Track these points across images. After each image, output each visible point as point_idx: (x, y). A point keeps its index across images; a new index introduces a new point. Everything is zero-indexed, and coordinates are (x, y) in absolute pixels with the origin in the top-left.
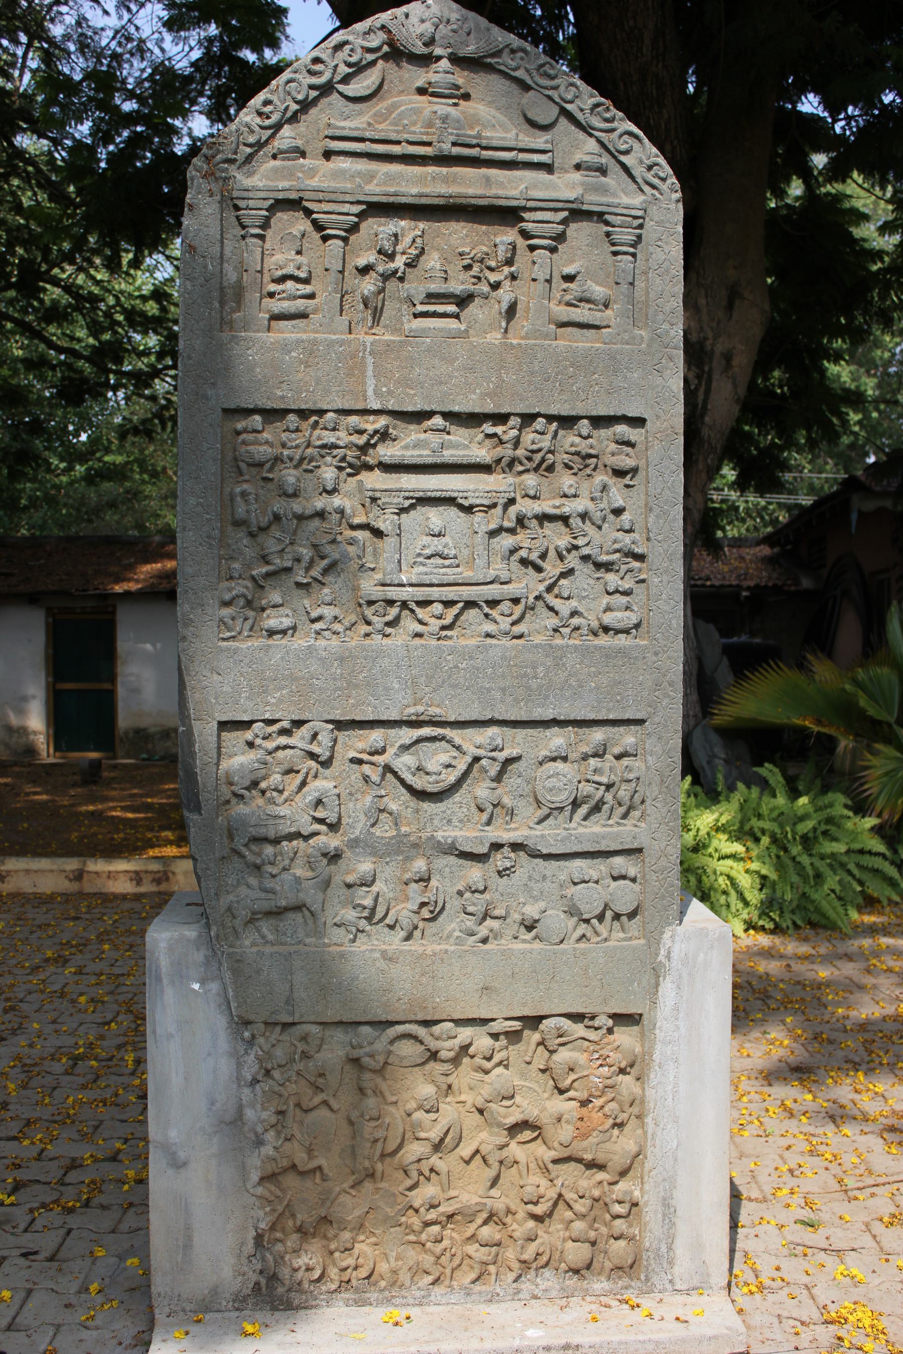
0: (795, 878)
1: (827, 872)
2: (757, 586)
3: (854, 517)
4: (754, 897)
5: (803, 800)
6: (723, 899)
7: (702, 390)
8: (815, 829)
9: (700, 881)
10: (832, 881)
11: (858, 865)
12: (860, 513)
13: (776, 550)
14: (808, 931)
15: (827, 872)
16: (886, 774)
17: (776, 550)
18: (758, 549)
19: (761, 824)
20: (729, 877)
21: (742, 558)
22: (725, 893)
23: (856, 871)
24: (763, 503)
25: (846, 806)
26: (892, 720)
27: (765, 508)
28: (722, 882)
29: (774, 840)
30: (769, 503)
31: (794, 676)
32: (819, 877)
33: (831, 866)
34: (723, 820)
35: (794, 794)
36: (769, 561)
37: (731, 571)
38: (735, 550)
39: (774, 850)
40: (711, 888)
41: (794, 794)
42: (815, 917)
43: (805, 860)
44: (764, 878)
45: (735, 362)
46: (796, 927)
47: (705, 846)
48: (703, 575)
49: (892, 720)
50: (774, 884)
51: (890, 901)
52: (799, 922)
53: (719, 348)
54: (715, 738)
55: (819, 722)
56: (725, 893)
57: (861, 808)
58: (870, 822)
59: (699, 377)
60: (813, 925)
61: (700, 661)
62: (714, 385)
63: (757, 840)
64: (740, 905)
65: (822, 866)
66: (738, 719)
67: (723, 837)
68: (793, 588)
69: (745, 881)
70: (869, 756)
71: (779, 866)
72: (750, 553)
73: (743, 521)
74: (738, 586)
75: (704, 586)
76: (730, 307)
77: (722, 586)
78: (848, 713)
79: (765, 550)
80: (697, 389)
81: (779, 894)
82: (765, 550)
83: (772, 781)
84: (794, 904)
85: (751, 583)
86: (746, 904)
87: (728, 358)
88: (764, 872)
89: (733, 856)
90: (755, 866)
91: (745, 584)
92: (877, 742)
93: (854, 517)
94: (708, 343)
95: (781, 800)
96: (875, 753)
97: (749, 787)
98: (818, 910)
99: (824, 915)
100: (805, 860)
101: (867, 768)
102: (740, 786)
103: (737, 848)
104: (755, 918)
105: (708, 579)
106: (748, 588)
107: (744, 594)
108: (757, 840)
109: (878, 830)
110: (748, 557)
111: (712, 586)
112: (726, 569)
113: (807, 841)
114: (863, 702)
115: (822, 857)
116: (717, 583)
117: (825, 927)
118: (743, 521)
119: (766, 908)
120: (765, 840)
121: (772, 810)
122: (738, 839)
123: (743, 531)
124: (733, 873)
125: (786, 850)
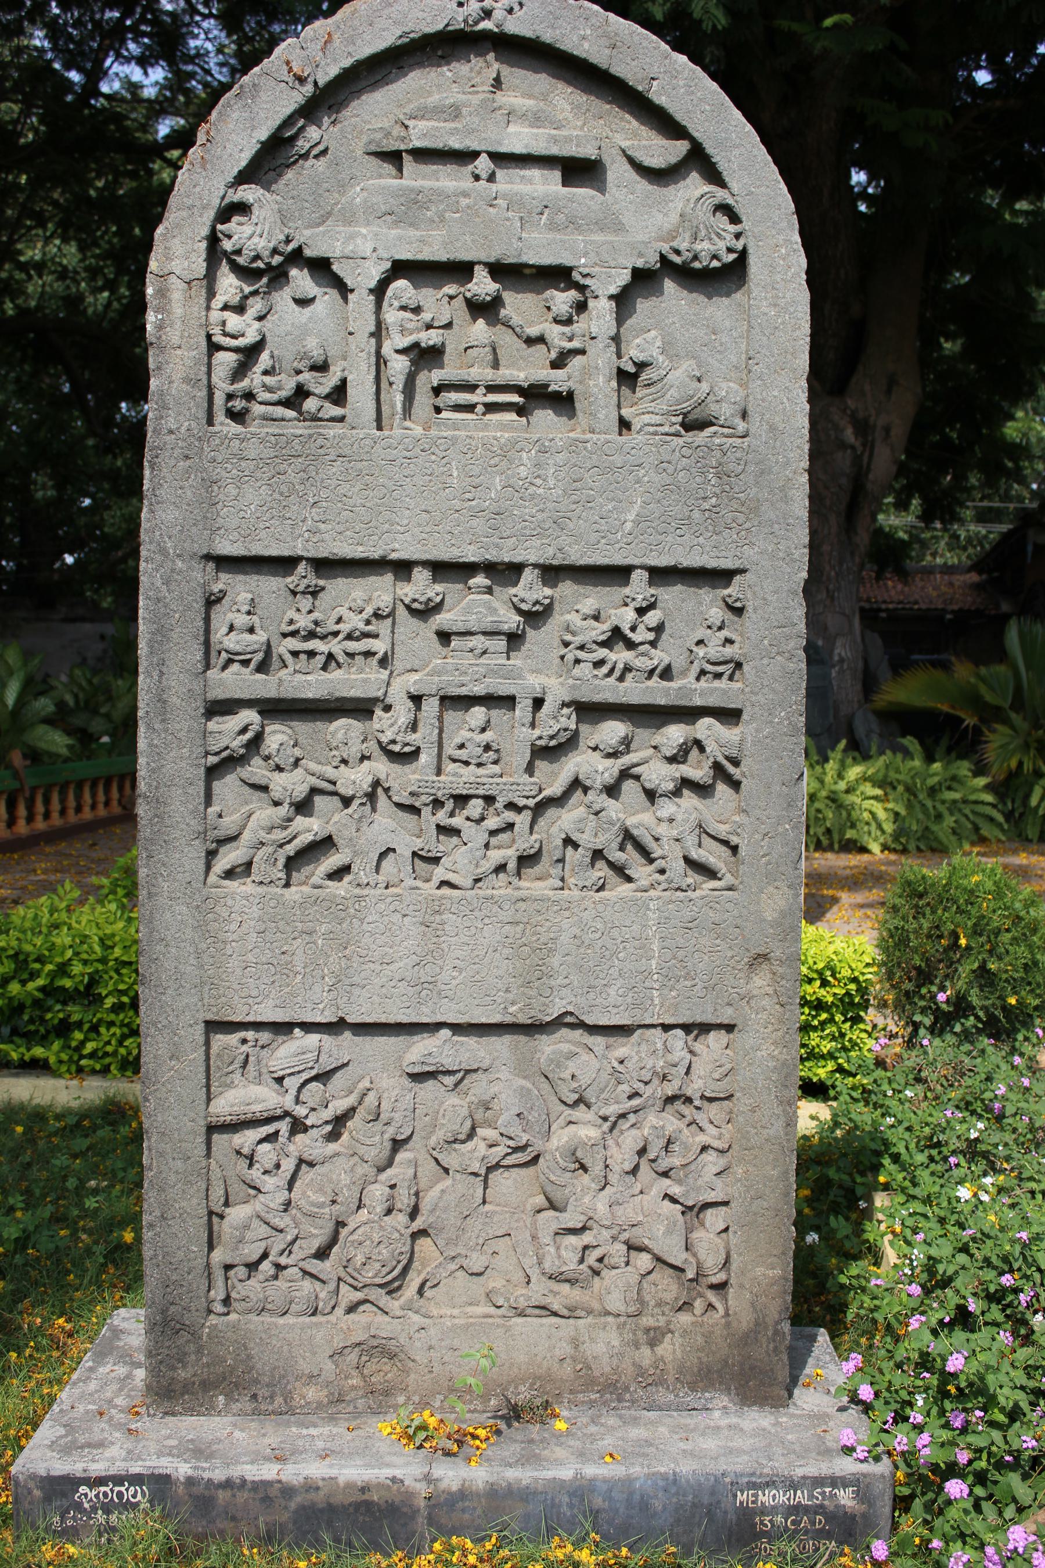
0: (921, 816)
1: (946, 813)
2: (961, 610)
3: (1030, 548)
4: (889, 827)
5: (937, 766)
6: (866, 828)
7: (866, 455)
8: (940, 783)
9: (849, 815)
10: (949, 821)
11: (973, 812)
12: (1036, 546)
13: (984, 577)
14: (929, 854)
15: (946, 813)
16: (1001, 747)
17: (984, 577)
18: (968, 576)
19: (898, 776)
20: (871, 812)
21: (951, 584)
22: (867, 824)
23: (971, 816)
24: (984, 532)
25: (970, 770)
26: (1006, 705)
27: (986, 537)
28: (866, 815)
29: (908, 789)
30: (990, 532)
31: (938, 674)
32: (939, 817)
33: (949, 809)
34: (870, 773)
35: (930, 759)
36: (977, 587)
37: (938, 596)
38: (946, 577)
39: (906, 795)
40: (858, 820)
41: (930, 759)
42: (934, 845)
43: (929, 803)
44: (897, 814)
45: (893, 433)
46: (919, 849)
47: (854, 790)
48: (912, 599)
49: (1006, 705)
50: (904, 819)
51: (999, 841)
52: (922, 847)
53: (881, 423)
54: (872, 718)
55: (953, 707)
56: (867, 824)
57: (978, 772)
58: (982, 781)
59: (864, 445)
60: (933, 850)
61: (866, 661)
62: (876, 450)
63: (894, 788)
64: (879, 833)
65: (942, 808)
66: (890, 703)
67: (868, 784)
68: (993, 612)
69: (882, 815)
70: (987, 733)
71: (909, 806)
72: (959, 579)
73: (965, 549)
74: (943, 610)
75: (911, 609)
76: (889, 392)
77: (928, 610)
78: (975, 701)
79: (974, 577)
80: (862, 454)
81: (907, 825)
82: (974, 577)
83: (911, 749)
84: (919, 834)
85: (956, 607)
86: (883, 832)
87: (887, 430)
88: (897, 809)
89: (875, 798)
90: (890, 806)
91: (950, 608)
92: (997, 722)
93: (1030, 548)
94: (872, 419)
95: (917, 763)
96: (994, 731)
97: (894, 753)
98: (936, 839)
99: (941, 843)
100: (929, 803)
101: (986, 742)
102: (889, 752)
103: (879, 792)
104: (889, 843)
105: (916, 603)
106: (953, 612)
107: (949, 616)
108: (894, 788)
109: (988, 788)
110: (957, 584)
111: (919, 609)
112: (935, 594)
113: (933, 791)
114: (983, 690)
115: (943, 802)
116: (924, 606)
117: (941, 851)
118: (965, 549)
119: (896, 836)
120: (900, 788)
121: (910, 770)
122: (880, 787)
123: (964, 558)
124: (874, 809)
125: (915, 796)
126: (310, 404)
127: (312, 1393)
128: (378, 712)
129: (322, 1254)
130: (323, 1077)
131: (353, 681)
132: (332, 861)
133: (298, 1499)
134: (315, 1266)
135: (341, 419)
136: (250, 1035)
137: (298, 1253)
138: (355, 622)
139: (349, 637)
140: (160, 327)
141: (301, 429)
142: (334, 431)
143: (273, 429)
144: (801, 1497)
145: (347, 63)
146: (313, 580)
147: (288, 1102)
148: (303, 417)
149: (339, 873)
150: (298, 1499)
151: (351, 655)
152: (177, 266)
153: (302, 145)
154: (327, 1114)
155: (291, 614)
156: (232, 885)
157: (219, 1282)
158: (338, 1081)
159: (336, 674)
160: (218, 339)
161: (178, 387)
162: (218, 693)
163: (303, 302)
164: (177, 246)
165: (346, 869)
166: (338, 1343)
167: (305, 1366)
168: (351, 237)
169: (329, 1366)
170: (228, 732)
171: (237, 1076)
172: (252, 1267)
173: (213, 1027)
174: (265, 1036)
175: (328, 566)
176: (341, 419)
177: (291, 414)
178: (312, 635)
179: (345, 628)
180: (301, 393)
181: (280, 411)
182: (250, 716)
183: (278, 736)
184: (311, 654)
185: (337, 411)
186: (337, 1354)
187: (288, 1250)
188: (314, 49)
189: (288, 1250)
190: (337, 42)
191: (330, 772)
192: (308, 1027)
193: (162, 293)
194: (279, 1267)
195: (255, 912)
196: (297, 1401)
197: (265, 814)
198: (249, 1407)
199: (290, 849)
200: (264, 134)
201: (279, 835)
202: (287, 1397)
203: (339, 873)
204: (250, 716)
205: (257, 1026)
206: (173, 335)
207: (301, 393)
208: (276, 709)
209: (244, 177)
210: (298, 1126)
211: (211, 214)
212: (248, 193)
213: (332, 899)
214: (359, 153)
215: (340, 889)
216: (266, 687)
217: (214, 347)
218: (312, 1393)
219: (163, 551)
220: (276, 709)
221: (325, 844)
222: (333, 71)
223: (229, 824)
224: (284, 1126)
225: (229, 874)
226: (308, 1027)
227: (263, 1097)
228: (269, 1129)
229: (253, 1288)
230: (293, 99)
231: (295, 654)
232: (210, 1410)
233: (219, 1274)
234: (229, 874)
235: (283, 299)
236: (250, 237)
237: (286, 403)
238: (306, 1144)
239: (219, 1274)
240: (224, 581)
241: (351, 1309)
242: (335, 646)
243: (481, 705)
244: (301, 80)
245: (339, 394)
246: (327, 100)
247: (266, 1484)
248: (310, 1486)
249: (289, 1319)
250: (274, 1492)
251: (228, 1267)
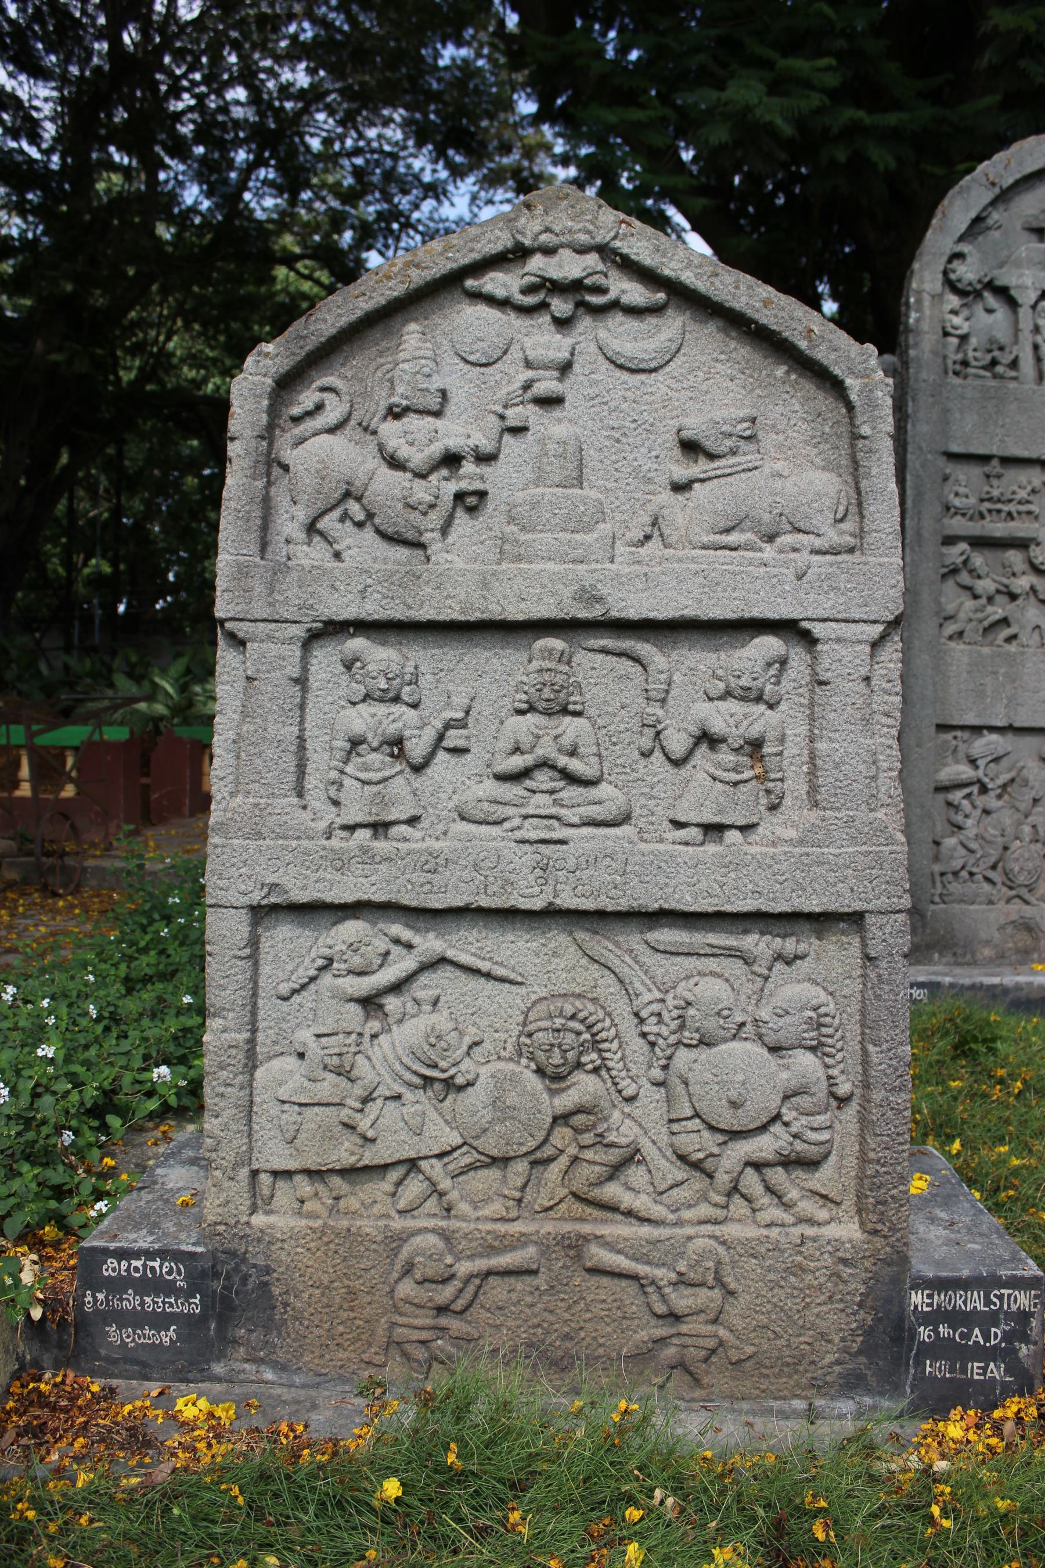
126: (1000, 369)
127: (987, 952)
128: (1033, 547)
129: (994, 867)
130: (996, 760)
131: (1019, 528)
132: (1007, 632)
133: (1011, 996)
134: (991, 874)
135: (1015, 379)
136: (959, 733)
137: (982, 866)
138: (1022, 494)
139: (1020, 503)
140: (918, 320)
141: (994, 383)
142: (1012, 385)
143: (978, 382)
144: (776, 1404)
145: (1018, 176)
146: (999, 469)
147: (980, 773)
148: (995, 376)
149: (1010, 639)
150: (1011, 996)
151: (1019, 513)
152: (927, 287)
153: (990, 222)
154: (1000, 781)
155: (987, 488)
156: (953, 644)
157: (939, 885)
158: (1004, 763)
159: (1012, 524)
160: (950, 330)
161: (927, 356)
162: (949, 532)
163: (990, 311)
164: (927, 275)
165: (1014, 637)
166: (1002, 921)
167: (983, 935)
168: (1021, 275)
169: (997, 935)
170: (956, 553)
171: (949, 760)
172: (955, 874)
173: (942, 728)
174: (966, 735)
175: (1008, 461)
176: (1015, 379)
177: (988, 374)
178: (999, 501)
179: (1018, 497)
180: (994, 363)
181: (982, 372)
182: (963, 546)
183: (978, 560)
184: (999, 511)
185: (1013, 374)
186: (1002, 928)
187: (976, 864)
188: (1000, 167)
189: (976, 864)
190: (1013, 164)
191: (1005, 581)
192: (992, 729)
193: (919, 301)
194: (971, 874)
195: (965, 659)
196: (979, 956)
197: (970, 604)
198: (952, 960)
199: (986, 623)
200: (973, 214)
201: (980, 615)
202: (973, 955)
203: (1010, 639)
204: (963, 546)
205: (963, 728)
206: (925, 326)
207: (994, 363)
208: (980, 543)
209: (961, 239)
210: (984, 790)
211: (945, 258)
212: (965, 248)
213: (1008, 653)
214: (1019, 228)
215: (1013, 648)
216: (975, 529)
217: (946, 334)
218: (987, 952)
219: (920, 448)
220: (980, 543)
221: (1005, 622)
222: (1010, 181)
223: (950, 608)
224: (975, 789)
225: (950, 638)
226: (992, 729)
227: (966, 772)
228: (966, 791)
229: (955, 887)
230: (988, 196)
231: (990, 511)
232: (930, 962)
233: (938, 879)
234: (950, 638)
235: (978, 309)
236: (967, 272)
237: (984, 368)
238: (990, 801)
239: (938, 879)
240: (950, 468)
241: (1008, 901)
242: (1012, 507)
243: (776, 635)
244: (993, 184)
245: (1014, 364)
246: (1004, 197)
247: (994, 986)
248: (1018, 987)
249: (975, 907)
250: (998, 991)
251: (942, 874)
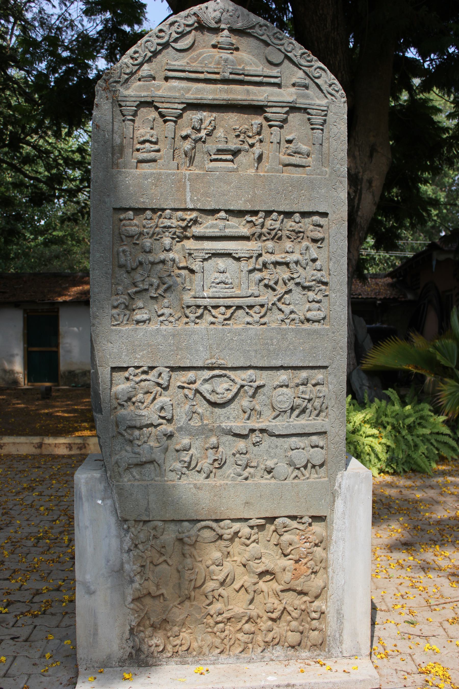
0: (404, 447)
1: (420, 444)
2: (385, 298)
3: (434, 263)
4: (383, 456)
5: (408, 407)
6: (367, 458)
7: (357, 198)
8: (414, 422)
9: (356, 448)
10: (423, 448)
11: (436, 440)
12: (437, 261)
13: (394, 280)
14: (411, 474)
15: (420, 444)
16: (451, 394)
17: (394, 280)
18: (385, 279)
19: (387, 419)
20: (370, 446)
21: (377, 284)
22: (368, 454)
23: (435, 443)
24: (388, 256)
25: (430, 410)
26: (453, 366)
27: (389, 259)
28: (367, 449)
29: (394, 427)
30: (391, 256)
31: (403, 344)
32: (416, 446)
33: (422, 441)
34: (368, 417)
35: (404, 404)
36: (391, 285)
37: (372, 291)
38: (373, 280)
39: (393, 432)
40: (362, 452)
41: (404, 404)
42: (414, 467)
43: (409, 438)
44: (388, 447)
45: (374, 184)
46: (405, 471)
47: (358, 431)
48: (357, 293)
49: (453, 366)
50: (393, 450)
51: (452, 458)
52: (406, 469)
53: (366, 177)
54: (363, 375)
55: (416, 367)
56: (368, 454)
57: (437, 411)
58: (442, 418)
59: (355, 192)
60: (413, 471)
61: (356, 336)
62: (363, 196)
63: (385, 427)
64: (376, 461)
65: (418, 441)
66: (375, 366)
67: (368, 426)
68: (403, 299)
69: (379, 448)
70: (442, 385)
71: (396, 441)
72: (381, 281)
73: (378, 265)
74: (375, 298)
75: (358, 298)
76: (371, 156)
77: (367, 298)
78: (431, 363)
79: (389, 280)
80: (354, 198)
81: (396, 455)
82: (389, 280)
83: (392, 398)
84: (404, 460)
85: (382, 297)
86: (379, 460)
87: (370, 182)
88: (388, 444)
89: (372, 436)
90: (384, 441)
91: (379, 297)
92: (446, 377)
93: (434, 263)
94: (360, 175)
95: (397, 407)
96: (445, 383)
97: (381, 401)
98: (416, 463)
99: (419, 466)
100: (409, 438)
101: (441, 391)
102: (376, 400)
103: (375, 431)
104: (384, 467)
105: (360, 295)
106: (380, 299)
107: (378, 302)
108: (385, 427)
109: (446, 423)
110: (380, 284)
111: (362, 298)
112: (369, 289)
113: (410, 428)
114: (439, 357)
115: (418, 436)
116: (365, 297)
117: (419, 472)
118: (378, 265)
119: (389, 462)
120: (389, 428)
121: (392, 412)
122: (375, 427)
123: (378, 270)
124: (373, 444)
125: (399, 432)
